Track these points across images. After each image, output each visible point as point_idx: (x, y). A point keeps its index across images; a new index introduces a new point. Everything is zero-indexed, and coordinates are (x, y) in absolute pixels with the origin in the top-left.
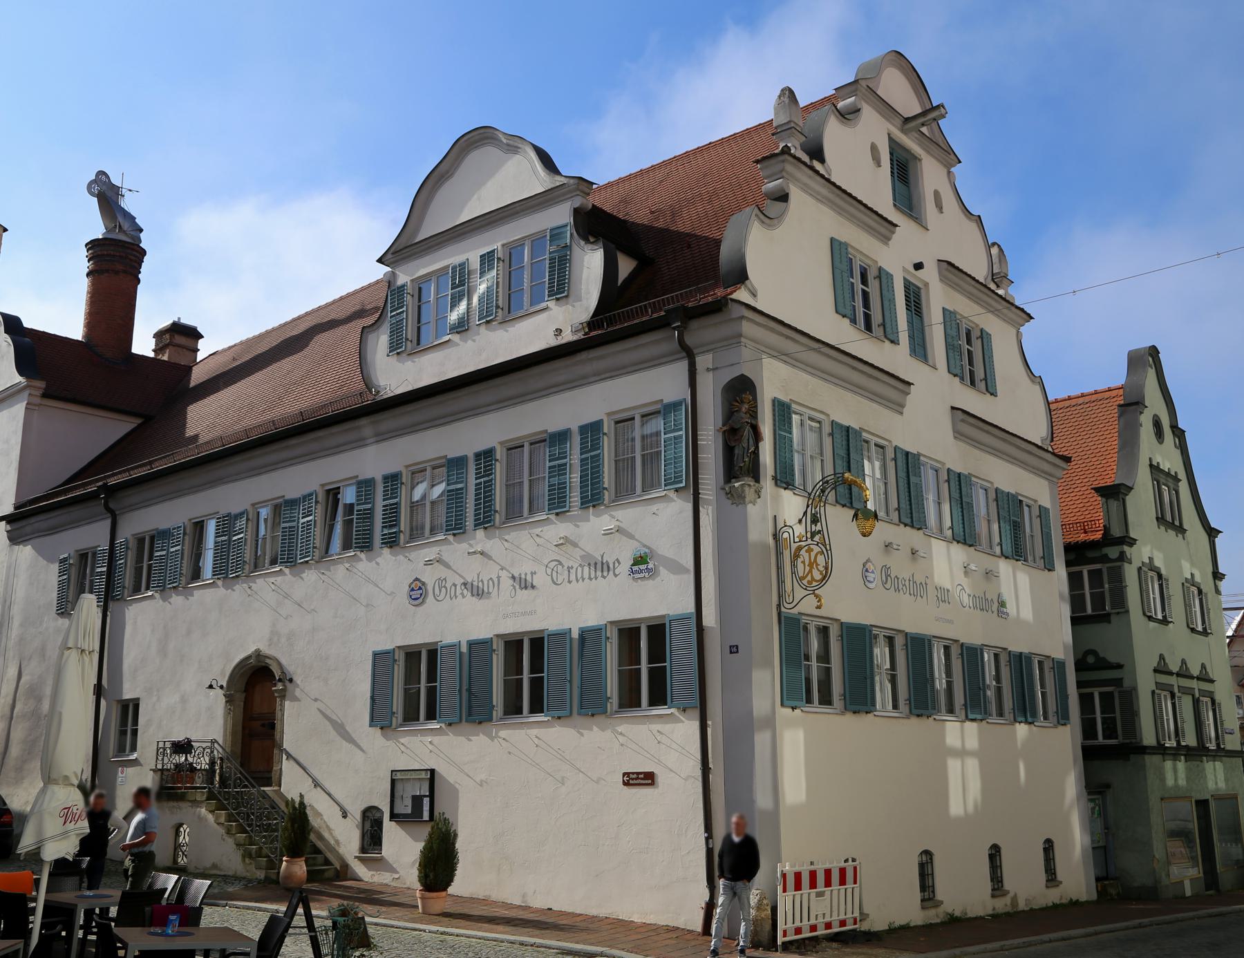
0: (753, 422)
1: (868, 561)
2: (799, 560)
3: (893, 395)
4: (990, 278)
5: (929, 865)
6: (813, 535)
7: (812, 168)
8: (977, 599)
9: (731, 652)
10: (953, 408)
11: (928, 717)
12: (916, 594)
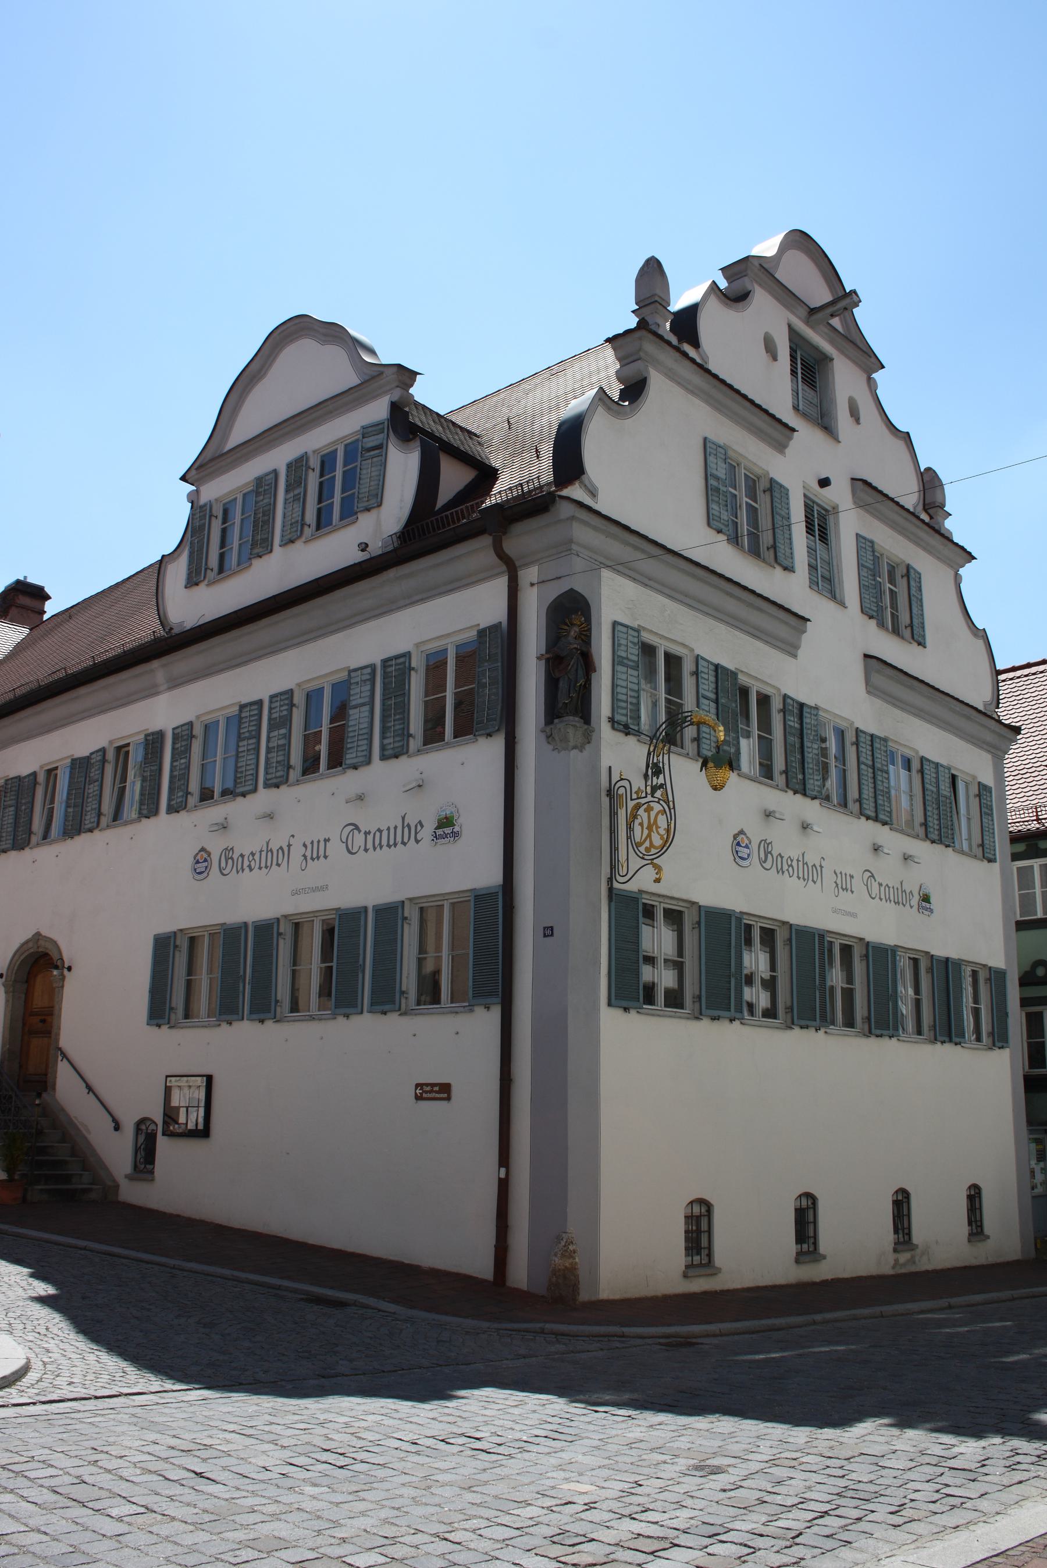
0: (584, 649)
1: (742, 832)
2: (637, 822)
3: (783, 632)
4: (921, 507)
5: (811, 1212)
6: (654, 789)
7: (677, 349)
8: (891, 889)
9: (545, 936)
10: (866, 656)
11: (816, 1030)
12: (806, 877)
